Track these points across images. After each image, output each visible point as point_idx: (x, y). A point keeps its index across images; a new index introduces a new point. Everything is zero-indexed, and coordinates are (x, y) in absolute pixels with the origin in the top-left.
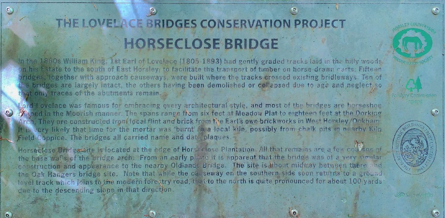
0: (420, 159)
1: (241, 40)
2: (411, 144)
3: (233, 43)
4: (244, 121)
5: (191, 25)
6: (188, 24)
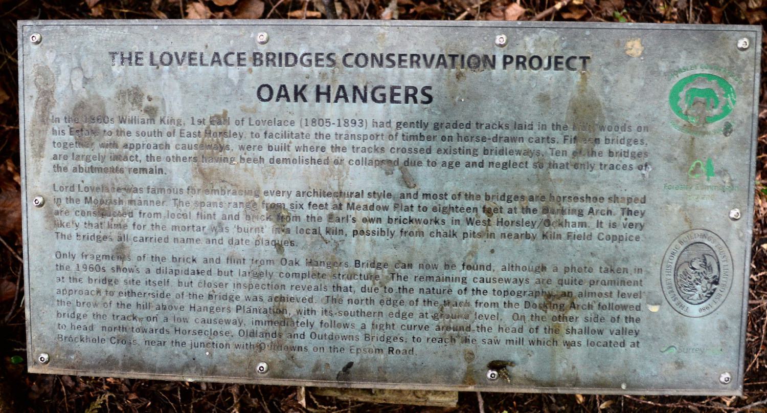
0: (704, 292)
1: (274, 55)
2: (693, 268)
3: (264, 59)
4: (359, 219)
5: (326, 62)
6: (322, 60)
